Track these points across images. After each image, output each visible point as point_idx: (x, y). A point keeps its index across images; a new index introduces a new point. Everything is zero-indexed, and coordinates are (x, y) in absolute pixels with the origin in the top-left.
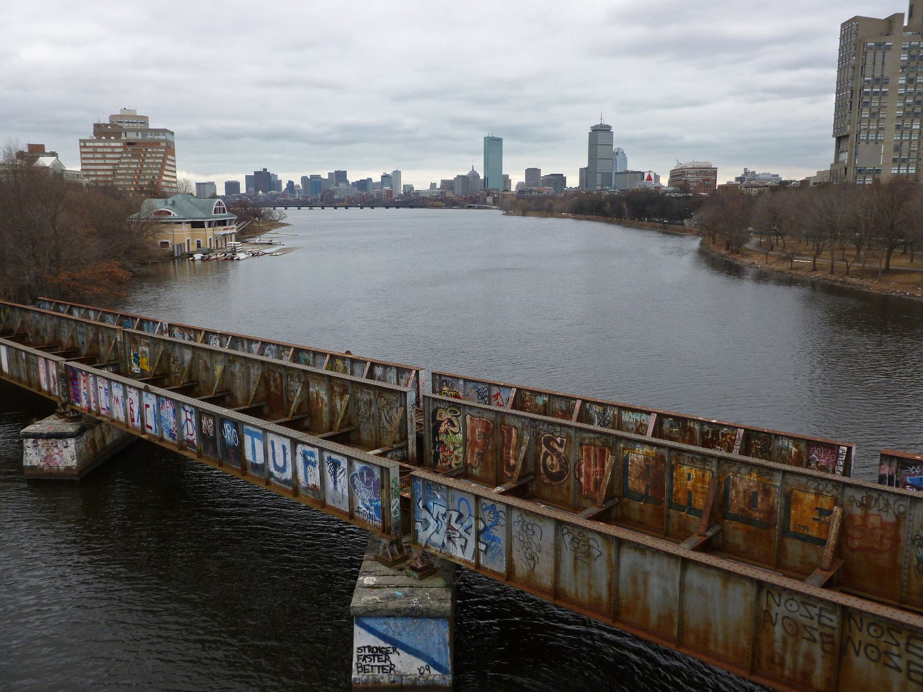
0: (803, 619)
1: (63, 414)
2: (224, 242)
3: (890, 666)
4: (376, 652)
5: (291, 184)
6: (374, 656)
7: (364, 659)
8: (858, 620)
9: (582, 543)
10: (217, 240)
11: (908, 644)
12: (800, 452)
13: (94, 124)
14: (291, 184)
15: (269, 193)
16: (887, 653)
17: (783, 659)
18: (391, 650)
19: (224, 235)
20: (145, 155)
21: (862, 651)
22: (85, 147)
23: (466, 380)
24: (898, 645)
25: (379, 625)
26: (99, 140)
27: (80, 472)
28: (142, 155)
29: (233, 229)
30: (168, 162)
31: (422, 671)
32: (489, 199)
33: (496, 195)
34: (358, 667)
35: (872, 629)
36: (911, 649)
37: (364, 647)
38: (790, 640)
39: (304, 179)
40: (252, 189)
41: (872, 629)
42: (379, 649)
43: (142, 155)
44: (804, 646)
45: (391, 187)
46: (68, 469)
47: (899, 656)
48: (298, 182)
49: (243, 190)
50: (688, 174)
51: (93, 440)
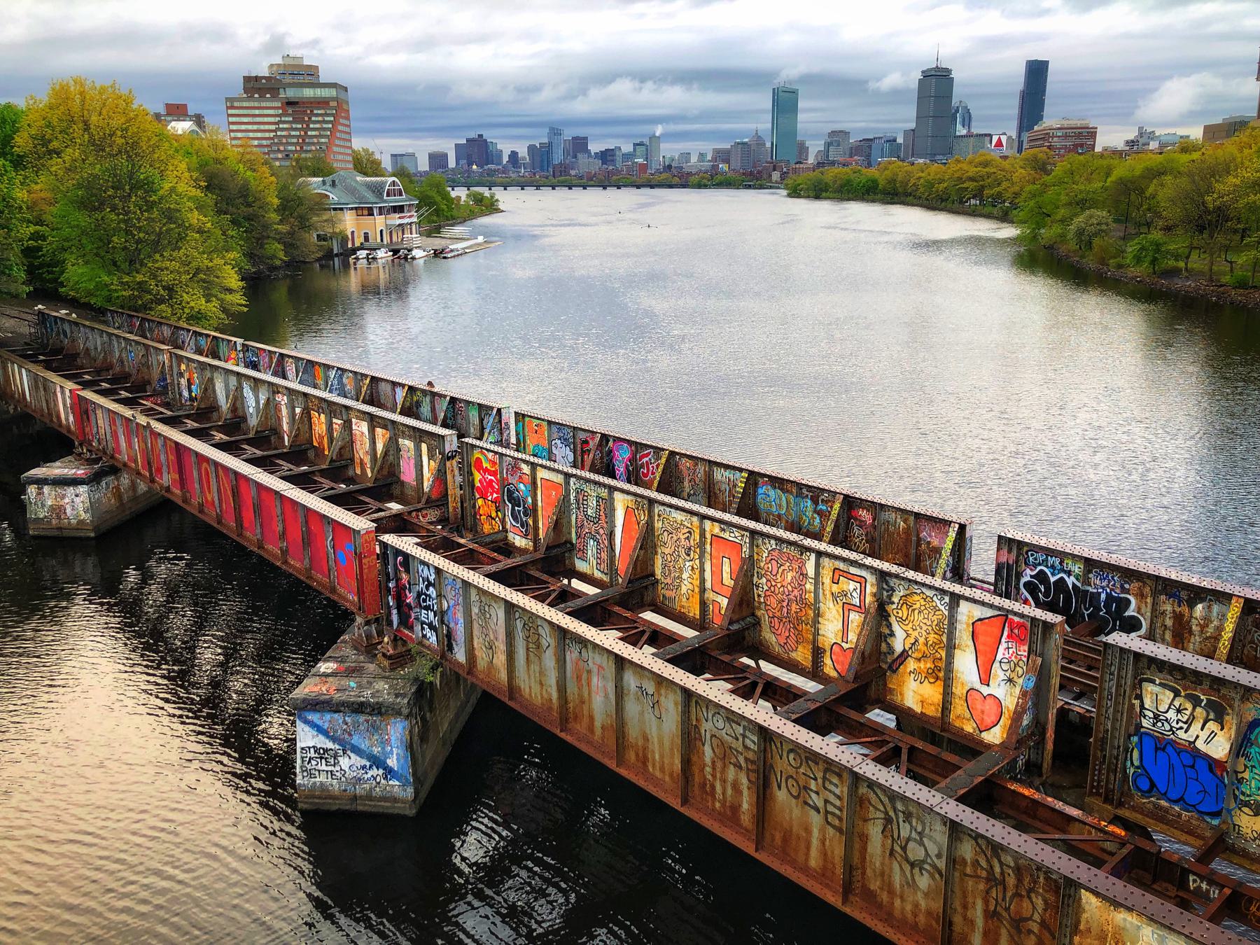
0: (728, 738)
1: (80, 455)
2: (400, 234)
3: (809, 805)
4: (322, 754)
5: (514, 155)
6: (321, 758)
7: (309, 762)
8: (779, 745)
9: (532, 630)
10: (391, 232)
11: (824, 778)
12: (909, 527)
13: (1046, 63)
14: (514, 155)
15: (486, 167)
16: (806, 788)
17: (713, 787)
18: (341, 752)
19: (400, 225)
20: (310, 118)
21: (783, 784)
22: (232, 107)
23: (550, 423)
24: (816, 779)
25: (325, 719)
26: (251, 98)
27: (95, 529)
28: (306, 119)
29: (412, 217)
30: (340, 128)
31: (378, 780)
32: (776, 176)
33: (785, 170)
34: (303, 771)
35: (792, 756)
36: (827, 784)
37: (309, 748)
38: (719, 765)
39: (531, 149)
40: (463, 162)
41: (792, 756)
42: (326, 750)
43: (306, 119)
44: (731, 773)
45: (646, 159)
46: (81, 522)
47: (817, 793)
48: (523, 152)
49: (452, 163)
50: (1053, 137)
51: (117, 488)
